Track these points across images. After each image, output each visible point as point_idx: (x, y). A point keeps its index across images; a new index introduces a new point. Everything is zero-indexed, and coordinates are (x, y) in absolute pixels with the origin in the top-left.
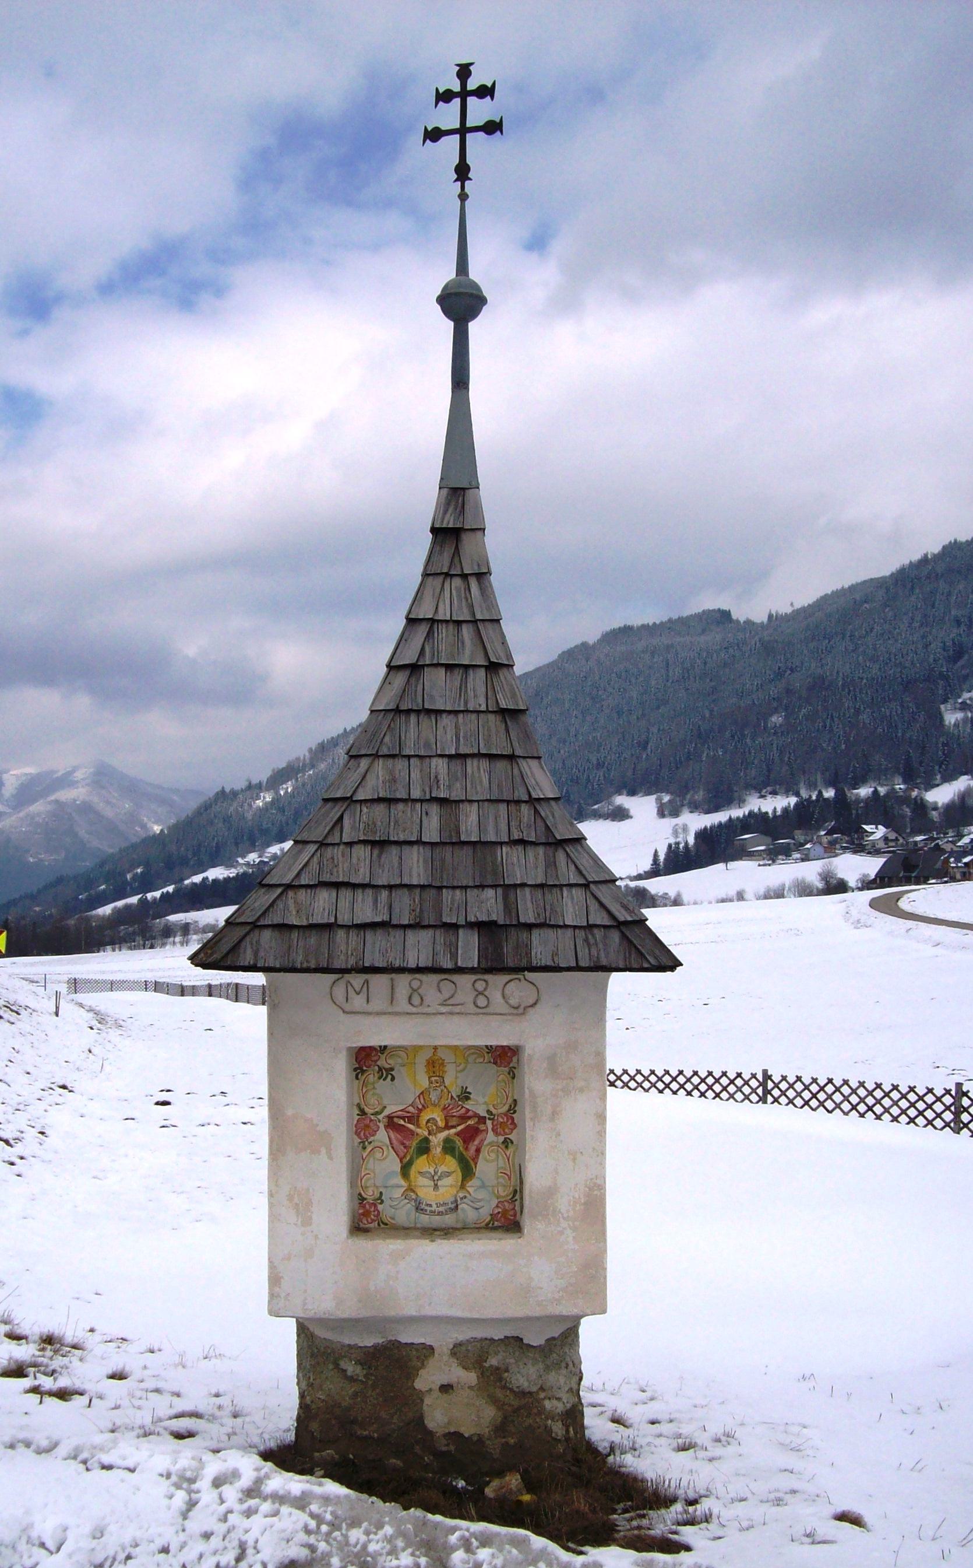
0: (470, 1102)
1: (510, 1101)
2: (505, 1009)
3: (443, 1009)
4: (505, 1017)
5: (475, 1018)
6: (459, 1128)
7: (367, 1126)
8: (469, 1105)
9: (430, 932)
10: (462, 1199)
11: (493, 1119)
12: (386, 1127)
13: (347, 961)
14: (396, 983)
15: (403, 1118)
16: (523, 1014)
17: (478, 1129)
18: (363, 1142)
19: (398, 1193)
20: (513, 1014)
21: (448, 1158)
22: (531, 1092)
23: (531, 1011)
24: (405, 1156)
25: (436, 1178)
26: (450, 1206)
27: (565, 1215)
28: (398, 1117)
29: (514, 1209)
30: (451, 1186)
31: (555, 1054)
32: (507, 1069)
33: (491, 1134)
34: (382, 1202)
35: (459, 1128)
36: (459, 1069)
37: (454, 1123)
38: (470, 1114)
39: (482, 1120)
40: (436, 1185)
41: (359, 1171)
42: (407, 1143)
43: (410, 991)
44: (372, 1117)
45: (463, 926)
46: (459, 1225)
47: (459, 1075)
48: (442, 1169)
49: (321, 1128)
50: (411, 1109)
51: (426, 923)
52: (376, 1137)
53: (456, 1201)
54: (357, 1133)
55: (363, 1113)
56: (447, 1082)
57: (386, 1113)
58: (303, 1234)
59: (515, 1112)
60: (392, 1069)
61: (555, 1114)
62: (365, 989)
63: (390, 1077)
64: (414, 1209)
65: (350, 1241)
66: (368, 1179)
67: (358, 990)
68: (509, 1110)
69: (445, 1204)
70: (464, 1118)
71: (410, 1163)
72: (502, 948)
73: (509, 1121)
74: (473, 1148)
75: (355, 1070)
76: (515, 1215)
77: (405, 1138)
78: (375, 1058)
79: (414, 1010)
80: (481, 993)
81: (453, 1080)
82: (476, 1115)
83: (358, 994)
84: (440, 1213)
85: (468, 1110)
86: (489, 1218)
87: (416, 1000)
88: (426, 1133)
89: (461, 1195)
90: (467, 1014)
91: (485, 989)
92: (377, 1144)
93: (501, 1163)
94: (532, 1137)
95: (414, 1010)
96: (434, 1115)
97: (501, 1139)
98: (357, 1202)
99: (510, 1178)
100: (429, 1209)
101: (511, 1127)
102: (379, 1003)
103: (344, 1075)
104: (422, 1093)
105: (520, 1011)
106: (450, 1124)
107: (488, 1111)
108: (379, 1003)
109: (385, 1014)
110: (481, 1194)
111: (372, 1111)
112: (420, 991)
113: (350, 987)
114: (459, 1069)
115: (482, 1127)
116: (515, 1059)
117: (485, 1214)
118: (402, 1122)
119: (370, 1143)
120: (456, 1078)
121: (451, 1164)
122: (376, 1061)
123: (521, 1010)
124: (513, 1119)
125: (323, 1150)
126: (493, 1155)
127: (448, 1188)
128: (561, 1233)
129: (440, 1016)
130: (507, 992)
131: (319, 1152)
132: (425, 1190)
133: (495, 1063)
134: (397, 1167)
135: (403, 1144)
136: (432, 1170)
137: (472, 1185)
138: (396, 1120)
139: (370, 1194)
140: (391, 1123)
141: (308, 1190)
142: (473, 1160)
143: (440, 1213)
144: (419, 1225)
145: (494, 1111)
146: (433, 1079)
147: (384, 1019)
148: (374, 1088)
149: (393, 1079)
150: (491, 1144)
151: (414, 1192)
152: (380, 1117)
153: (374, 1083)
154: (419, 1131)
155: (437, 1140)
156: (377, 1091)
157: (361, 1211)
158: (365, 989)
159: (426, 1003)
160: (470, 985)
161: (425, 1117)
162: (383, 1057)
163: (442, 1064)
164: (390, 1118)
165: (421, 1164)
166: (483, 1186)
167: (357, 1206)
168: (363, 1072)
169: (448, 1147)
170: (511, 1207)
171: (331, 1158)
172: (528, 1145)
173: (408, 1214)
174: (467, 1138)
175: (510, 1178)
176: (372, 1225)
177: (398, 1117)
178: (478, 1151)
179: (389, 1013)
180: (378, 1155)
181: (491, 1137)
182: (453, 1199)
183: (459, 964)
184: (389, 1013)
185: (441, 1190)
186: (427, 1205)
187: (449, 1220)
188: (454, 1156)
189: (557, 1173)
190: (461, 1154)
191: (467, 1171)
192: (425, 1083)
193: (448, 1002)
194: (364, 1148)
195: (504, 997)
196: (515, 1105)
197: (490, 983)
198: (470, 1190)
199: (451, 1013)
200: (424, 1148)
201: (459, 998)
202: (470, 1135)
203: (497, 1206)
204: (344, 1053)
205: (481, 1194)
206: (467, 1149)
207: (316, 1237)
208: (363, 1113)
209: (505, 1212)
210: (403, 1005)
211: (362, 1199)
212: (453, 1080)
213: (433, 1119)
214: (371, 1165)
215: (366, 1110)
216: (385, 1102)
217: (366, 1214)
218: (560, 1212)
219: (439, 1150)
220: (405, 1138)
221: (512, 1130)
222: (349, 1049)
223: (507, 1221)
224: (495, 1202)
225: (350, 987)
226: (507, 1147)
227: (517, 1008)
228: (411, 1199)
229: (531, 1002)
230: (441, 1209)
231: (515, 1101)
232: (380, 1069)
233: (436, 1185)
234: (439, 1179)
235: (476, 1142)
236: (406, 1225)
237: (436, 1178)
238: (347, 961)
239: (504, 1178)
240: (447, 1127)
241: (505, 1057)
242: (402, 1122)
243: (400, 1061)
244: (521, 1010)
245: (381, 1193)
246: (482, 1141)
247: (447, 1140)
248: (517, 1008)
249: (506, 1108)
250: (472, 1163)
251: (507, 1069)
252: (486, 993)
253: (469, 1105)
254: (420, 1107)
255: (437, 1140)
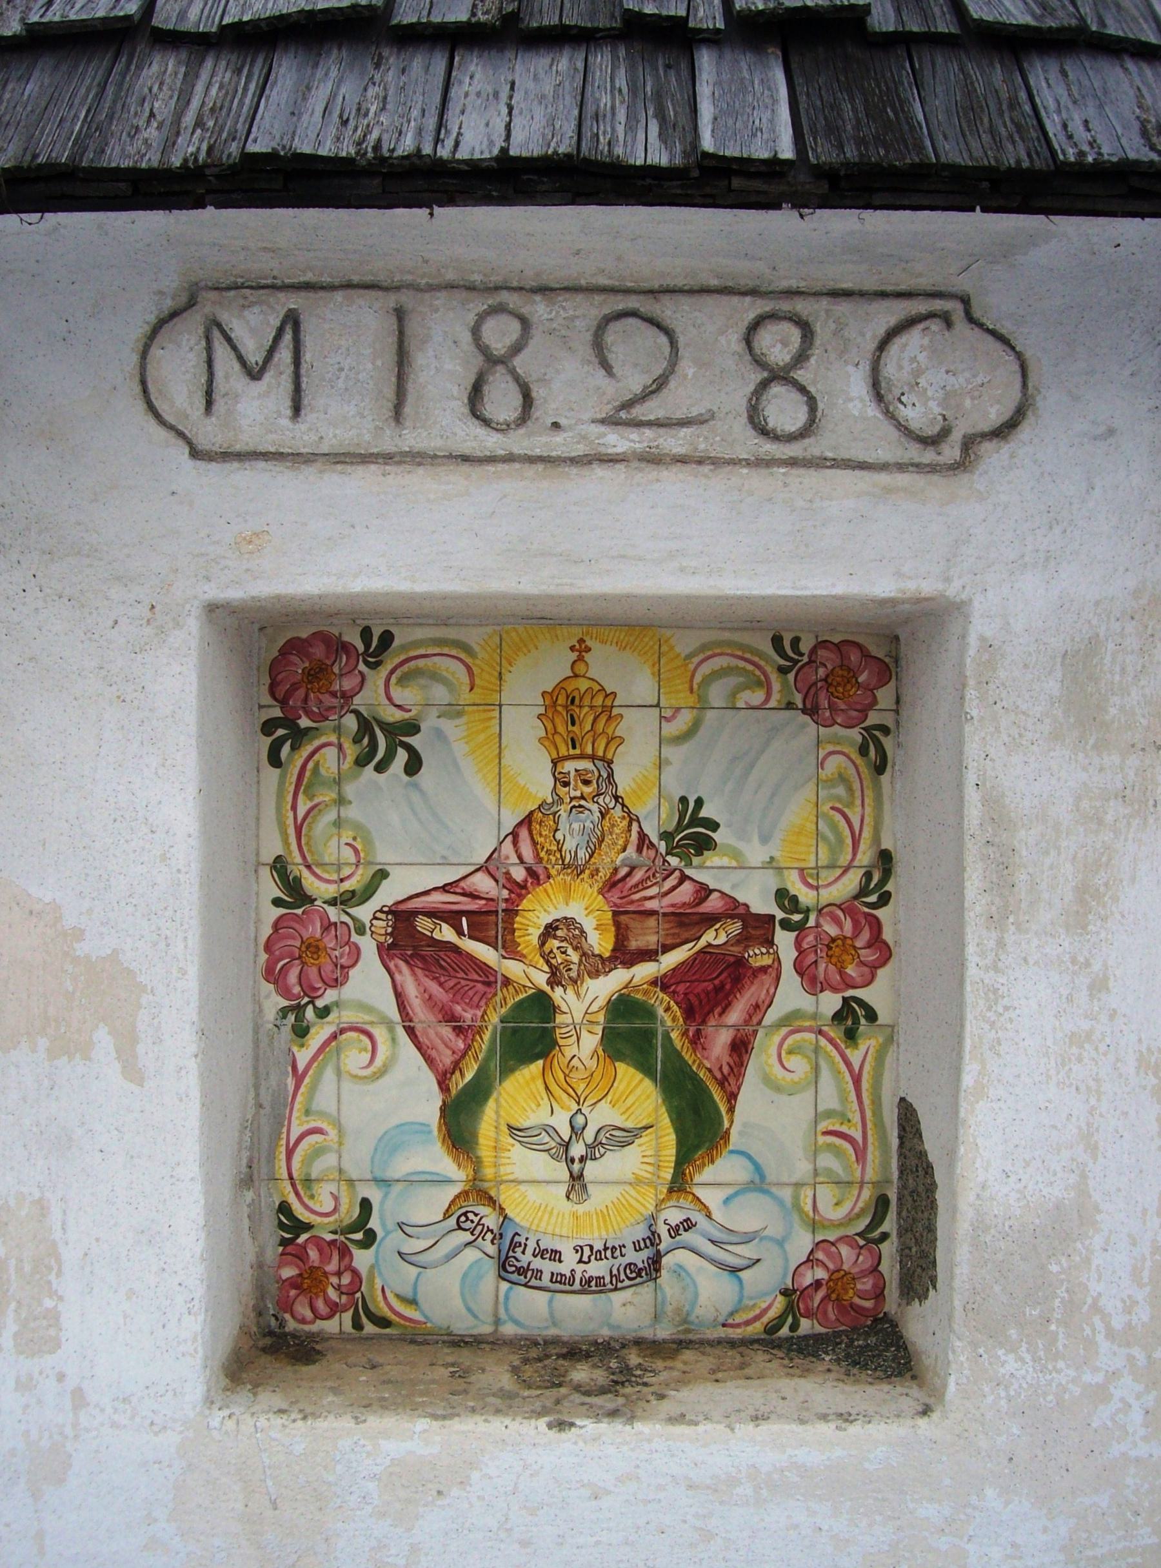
0: (712, 859)
1: (866, 856)
2: (885, 445)
3: (617, 441)
4: (883, 478)
5: (757, 480)
6: (671, 960)
7: (313, 948)
8: (709, 871)
9: (566, 62)
10: (674, 1231)
11: (800, 927)
12: (385, 952)
13: (169, 144)
14: (413, 326)
15: (452, 917)
16: (962, 465)
17: (740, 963)
18: (299, 1009)
19: (429, 1206)
20: (918, 467)
21: (626, 1073)
22: (993, 803)
23: (994, 456)
24: (456, 1066)
25: (577, 1150)
26: (632, 1256)
27: (1117, 1322)
28: (432, 914)
29: (875, 1270)
30: (637, 1182)
31: (1094, 644)
32: (855, 734)
33: (790, 979)
34: (370, 1239)
35: (671, 960)
36: (670, 729)
37: (651, 940)
38: (713, 904)
39: (758, 928)
40: (577, 1179)
41: (280, 1120)
42: (468, 1016)
43: (478, 361)
44: (333, 913)
45: (713, 39)
46: (664, 1332)
47: (668, 751)
48: (601, 1116)
49: (92, 947)
50: (483, 883)
51: (550, 19)
52: (349, 991)
53: (653, 1239)
54: (273, 975)
55: (295, 894)
56: (624, 780)
57: (387, 895)
58: (25, 1385)
59: (885, 899)
60: (413, 728)
61: (1088, 902)
62: (284, 355)
63: (402, 756)
64: (490, 1269)
65: (217, 1417)
66: (319, 1152)
67: (255, 357)
68: (863, 892)
69: (611, 1250)
70: (687, 922)
71: (478, 1092)
72: (902, 106)
73: (854, 939)
74: (720, 1040)
75: (268, 727)
76: (879, 1295)
77: (457, 993)
78: (348, 684)
79: (492, 442)
80: (777, 376)
81: (647, 773)
82: (735, 910)
83: (254, 374)
84: (591, 1285)
85: (704, 891)
86: (780, 1303)
87: (502, 401)
88: (541, 979)
89: (674, 1216)
90: (716, 462)
91: (801, 358)
92: (349, 1016)
93: (829, 1099)
94: (993, 994)
95: (492, 442)
96: (575, 910)
97: (831, 1002)
98: (271, 1235)
99: (861, 1155)
100: (547, 1267)
101: (869, 956)
102: (344, 412)
103: (190, 718)
104: (527, 821)
105: (947, 452)
106: (634, 944)
107: (783, 896)
108: (344, 412)
109: (365, 459)
110: (749, 1216)
111: (331, 891)
112: (518, 362)
113: (222, 351)
114: (670, 729)
115: (758, 957)
116: (885, 697)
117: (764, 1287)
118: (446, 933)
119: (323, 1013)
120: (661, 764)
121: (636, 1098)
122: (347, 697)
123: (951, 452)
124: (876, 926)
125: (103, 1039)
126: (799, 1065)
127: (627, 1185)
128: (1100, 1393)
129: (599, 471)
130: (890, 369)
131: (85, 1050)
132: (533, 1194)
133: (811, 710)
134: (427, 1105)
135: (449, 1017)
136: (561, 1122)
137: (717, 1176)
138: (424, 925)
139: (324, 1207)
140: (404, 937)
141: (42, 1207)
142: (722, 1083)
143: (591, 1285)
144: (508, 1329)
145: (806, 897)
146: (569, 767)
147: (360, 482)
148: (341, 801)
149: (414, 766)
150: (790, 1020)
151: (492, 1201)
152: (364, 912)
153: (338, 782)
154: (513, 968)
155: (584, 1003)
156: (351, 812)
157: (288, 1272)
158: (284, 355)
159: (544, 412)
160: (733, 341)
161: (538, 912)
162: (376, 679)
163: (607, 710)
164: (402, 916)
165: (521, 1097)
166: (759, 1183)
167: (273, 1251)
168: (298, 736)
169: (627, 1033)
170: (865, 1261)
171: (133, 1072)
172: (971, 1028)
173: (468, 1280)
174: (693, 1009)
175: (861, 1155)
176: (330, 1326)
177: (432, 914)
178: (741, 1047)
179: (387, 458)
180: (354, 1057)
181: (791, 994)
182: (641, 1232)
183: (708, 144)
184: (387, 458)
185: (599, 1197)
186: (541, 1253)
187: (627, 1311)
188: (647, 1070)
189: (1093, 1150)
190: (672, 1053)
191: (699, 1126)
192: (541, 786)
193: (638, 412)
194: (301, 1032)
195: (879, 397)
196: (887, 874)
197: (823, 331)
198: (712, 1198)
199: (653, 459)
200: (532, 1034)
201: (680, 398)
202: (713, 986)
203: (810, 1261)
204: (193, 625)
205: (749, 1216)
206: (696, 1041)
207: (79, 1398)
208: (295, 894)
209: (839, 1279)
210: (443, 421)
211: (291, 1225)
212: (647, 773)
213: (569, 922)
214: (325, 1099)
215: (311, 884)
216: (384, 855)
217: (309, 1282)
218: (1096, 1308)
219: (590, 1041)
220: (457, 993)
221: (874, 968)
222: (212, 609)
223: (858, 1321)
224: (802, 1243)
225: (222, 351)
226: (851, 1035)
227: (932, 441)
228: (479, 1231)
229: (995, 414)
230: (597, 1269)
231: (885, 858)
232: (365, 726)
233: (577, 1179)
234: (593, 1151)
235: (735, 1016)
236: (463, 1326)
237: (577, 1150)
238: (169, 144)
239: (838, 1152)
240: (624, 955)
241: (849, 676)
242: (446, 933)
243: (440, 694)
244: (951, 452)
245: (366, 1205)
246: (758, 1009)
247: (623, 1007)
248: (932, 441)
249: (851, 882)
250: (717, 1095)
251: (855, 734)
252: (799, 375)
253: (709, 871)
254: (519, 874)
255: (584, 1003)
